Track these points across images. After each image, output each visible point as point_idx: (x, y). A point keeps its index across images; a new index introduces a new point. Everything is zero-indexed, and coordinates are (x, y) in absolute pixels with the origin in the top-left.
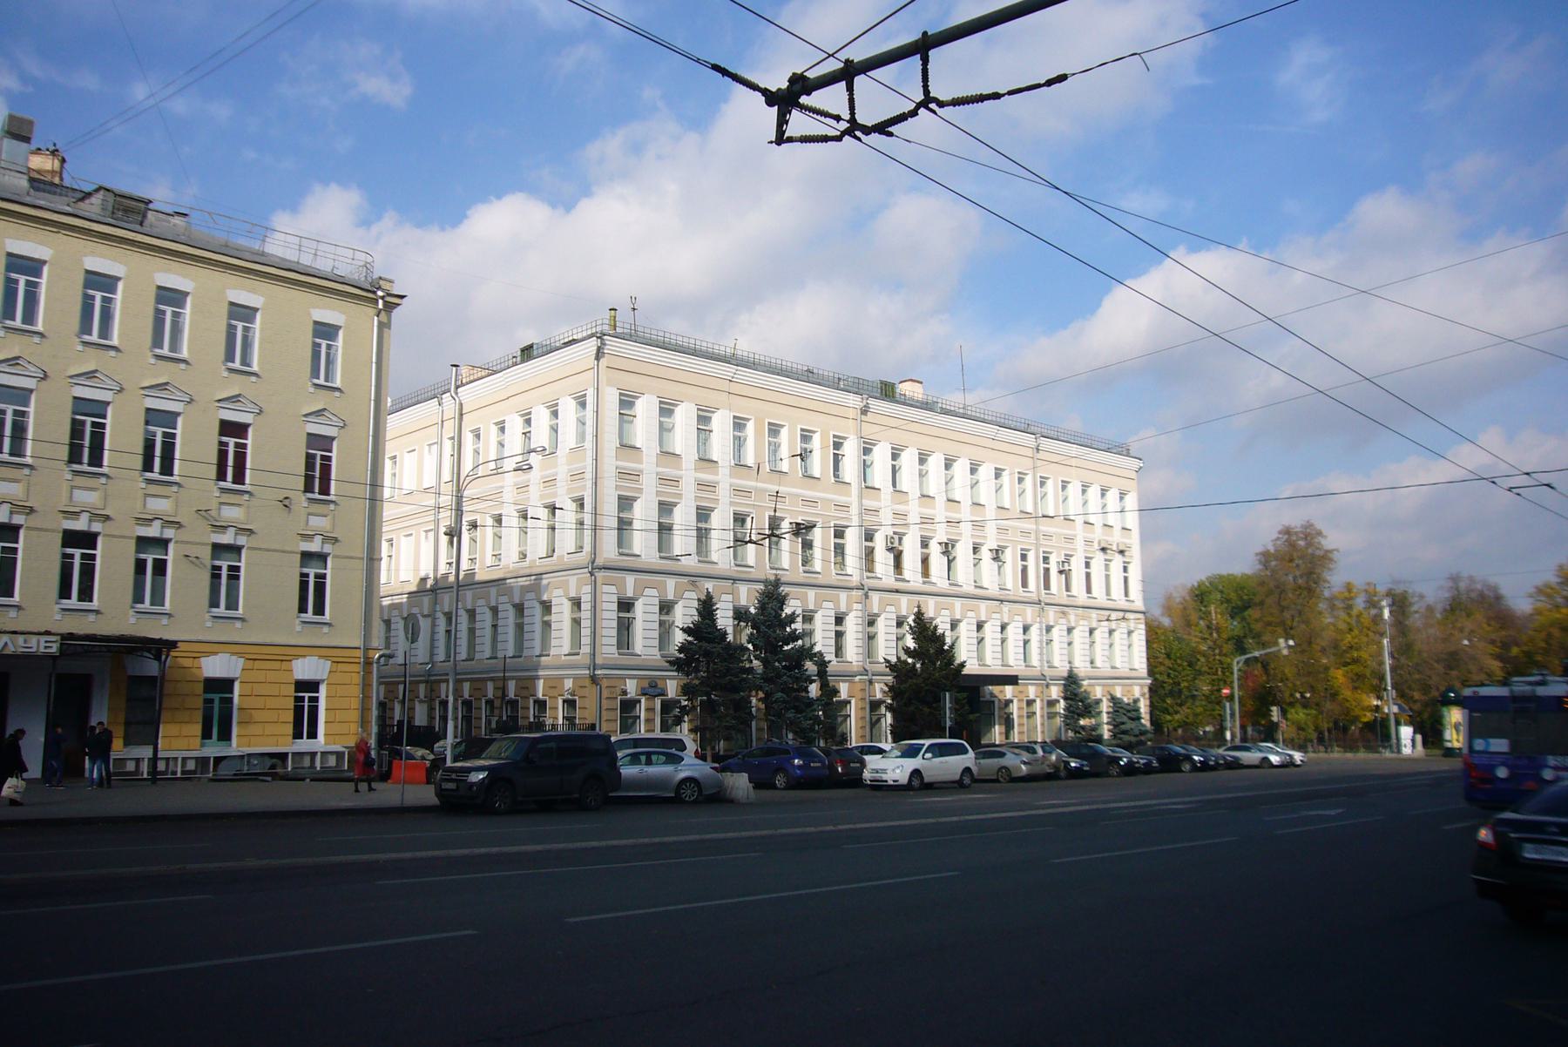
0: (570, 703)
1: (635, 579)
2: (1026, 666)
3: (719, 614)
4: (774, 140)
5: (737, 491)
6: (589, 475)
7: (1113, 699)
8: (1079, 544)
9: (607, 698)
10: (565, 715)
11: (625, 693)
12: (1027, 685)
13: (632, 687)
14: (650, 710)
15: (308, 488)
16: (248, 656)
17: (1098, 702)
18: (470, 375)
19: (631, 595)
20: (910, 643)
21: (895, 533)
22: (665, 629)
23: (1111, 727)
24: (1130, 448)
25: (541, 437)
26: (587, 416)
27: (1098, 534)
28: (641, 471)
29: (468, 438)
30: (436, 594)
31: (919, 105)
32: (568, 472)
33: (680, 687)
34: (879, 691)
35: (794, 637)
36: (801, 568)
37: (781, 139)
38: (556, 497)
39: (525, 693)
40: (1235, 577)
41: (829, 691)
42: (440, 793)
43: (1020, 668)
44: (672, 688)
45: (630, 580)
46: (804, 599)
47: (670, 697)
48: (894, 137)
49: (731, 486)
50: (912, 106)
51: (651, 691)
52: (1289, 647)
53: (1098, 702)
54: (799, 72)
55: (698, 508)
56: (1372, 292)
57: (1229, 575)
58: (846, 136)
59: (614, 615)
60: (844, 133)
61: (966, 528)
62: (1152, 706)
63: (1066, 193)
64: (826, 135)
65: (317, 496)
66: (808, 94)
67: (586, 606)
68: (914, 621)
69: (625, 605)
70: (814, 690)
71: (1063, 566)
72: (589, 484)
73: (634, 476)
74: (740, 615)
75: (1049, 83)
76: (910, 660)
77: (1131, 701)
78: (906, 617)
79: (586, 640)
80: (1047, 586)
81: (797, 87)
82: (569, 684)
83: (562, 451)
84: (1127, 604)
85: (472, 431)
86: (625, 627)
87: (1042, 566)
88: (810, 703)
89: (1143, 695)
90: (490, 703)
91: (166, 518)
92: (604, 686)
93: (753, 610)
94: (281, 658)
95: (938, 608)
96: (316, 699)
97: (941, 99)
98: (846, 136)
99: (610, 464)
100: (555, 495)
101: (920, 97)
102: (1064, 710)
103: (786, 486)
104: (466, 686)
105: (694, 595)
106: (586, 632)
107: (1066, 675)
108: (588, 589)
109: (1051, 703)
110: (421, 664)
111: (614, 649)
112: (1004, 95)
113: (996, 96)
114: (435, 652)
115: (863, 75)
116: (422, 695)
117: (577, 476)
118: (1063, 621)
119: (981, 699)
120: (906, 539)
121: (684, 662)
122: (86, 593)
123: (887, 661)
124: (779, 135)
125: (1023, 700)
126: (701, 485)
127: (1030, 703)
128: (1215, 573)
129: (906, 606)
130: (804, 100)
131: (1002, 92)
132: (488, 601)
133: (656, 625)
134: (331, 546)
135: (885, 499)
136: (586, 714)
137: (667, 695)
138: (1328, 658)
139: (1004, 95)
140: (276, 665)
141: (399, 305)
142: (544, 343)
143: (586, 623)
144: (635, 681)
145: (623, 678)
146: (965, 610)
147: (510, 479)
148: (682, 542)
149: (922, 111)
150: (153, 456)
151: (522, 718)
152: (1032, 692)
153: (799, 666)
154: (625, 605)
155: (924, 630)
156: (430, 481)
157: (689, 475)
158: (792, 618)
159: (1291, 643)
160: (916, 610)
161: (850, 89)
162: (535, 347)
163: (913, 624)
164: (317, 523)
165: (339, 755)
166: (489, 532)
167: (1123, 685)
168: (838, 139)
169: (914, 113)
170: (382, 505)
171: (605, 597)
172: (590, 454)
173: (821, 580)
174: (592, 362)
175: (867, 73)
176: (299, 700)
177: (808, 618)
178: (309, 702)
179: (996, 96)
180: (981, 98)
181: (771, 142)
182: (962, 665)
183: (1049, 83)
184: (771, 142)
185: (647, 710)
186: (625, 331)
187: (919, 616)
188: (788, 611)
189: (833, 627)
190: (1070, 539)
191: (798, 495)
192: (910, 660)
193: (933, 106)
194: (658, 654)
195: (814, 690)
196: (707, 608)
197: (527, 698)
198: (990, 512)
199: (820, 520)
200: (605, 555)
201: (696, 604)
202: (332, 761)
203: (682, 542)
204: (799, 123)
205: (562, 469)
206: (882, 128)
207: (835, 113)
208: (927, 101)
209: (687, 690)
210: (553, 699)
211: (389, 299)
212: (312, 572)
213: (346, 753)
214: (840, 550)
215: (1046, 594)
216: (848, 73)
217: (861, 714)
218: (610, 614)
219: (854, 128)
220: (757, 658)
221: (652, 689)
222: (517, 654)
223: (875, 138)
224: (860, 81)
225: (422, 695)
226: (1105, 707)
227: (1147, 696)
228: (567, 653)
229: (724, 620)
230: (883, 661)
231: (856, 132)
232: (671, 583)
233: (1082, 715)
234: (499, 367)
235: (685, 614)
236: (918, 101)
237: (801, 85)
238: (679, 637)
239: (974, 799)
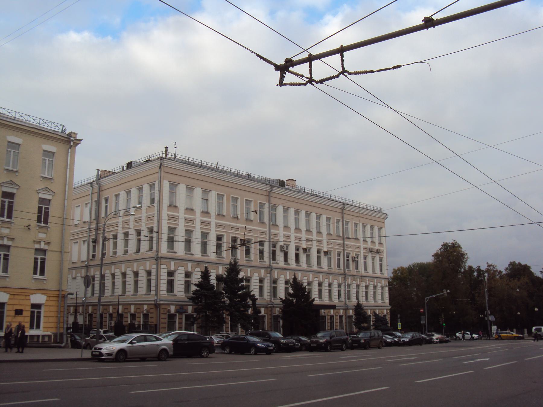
0: (146, 316)
1: (175, 263)
2: (339, 301)
3: (211, 278)
4: (279, 84)
5: (218, 225)
6: (156, 218)
7: (375, 315)
8: (362, 250)
10: (89, 320)
11: (169, 311)
12: (339, 309)
13: (173, 309)
14: (180, 319)
15: (39, 221)
16: (11, 293)
17: (370, 316)
18: (104, 174)
19: (190, 271)
20: (291, 291)
21: (284, 244)
22: (188, 284)
23: (374, 327)
24: (382, 209)
25: (134, 202)
26: (156, 193)
27: (369, 245)
28: (178, 217)
29: (103, 202)
30: (88, 268)
31: (340, 73)
32: (146, 217)
33: (193, 309)
34: (277, 311)
35: (243, 288)
36: (259, 260)
37: (281, 84)
38: (141, 227)
39: (126, 311)
40: (423, 264)
41: (257, 311)
42: (92, 355)
43: (337, 302)
44: (190, 309)
45: (173, 263)
46: (246, 272)
48: (323, 84)
49: (168, 215)
50: (337, 73)
52: (447, 293)
53: (370, 316)
54: (289, 58)
55: (202, 232)
56: (488, 146)
57: (421, 263)
58: (308, 83)
59: (166, 278)
60: (307, 82)
61: (315, 243)
62: (391, 318)
63: (392, 109)
64: (300, 86)
65: (42, 224)
66: (293, 67)
67: (153, 274)
68: (293, 281)
69: (171, 274)
70: (250, 311)
71: (355, 259)
72: (156, 222)
73: (193, 221)
74: (219, 278)
75: (394, 68)
76: (291, 299)
77: (382, 316)
78: (289, 280)
79: (153, 288)
80: (348, 267)
81: (288, 64)
82: (145, 307)
83: (144, 208)
84: (381, 275)
85: (105, 198)
86: (171, 284)
87: (346, 259)
88: (249, 317)
89: (387, 313)
90: (111, 315)
91: (9, 237)
93: (225, 276)
94: (25, 294)
95: (302, 276)
96: (39, 312)
97: (350, 72)
98: (308, 83)
99: (165, 212)
100: (141, 226)
101: (340, 70)
102: (355, 319)
103: (239, 224)
105: (199, 270)
106: (153, 285)
107: (356, 305)
108: (154, 266)
109: (350, 317)
110: (80, 298)
111: (165, 293)
112: (375, 72)
113: (372, 72)
114: (87, 293)
115: (319, 60)
116: (81, 311)
117: (150, 218)
118: (354, 282)
119: (320, 315)
120: (290, 248)
121: (196, 298)
122: (42, 273)
123: (281, 299)
124: (281, 82)
125: (337, 316)
126: (203, 223)
127: (341, 317)
128: (416, 262)
129: (289, 276)
130: (291, 69)
131: (374, 70)
132: (111, 271)
134: (48, 246)
135: (281, 232)
136: (153, 320)
139: (375, 72)
140: (23, 297)
141: (79, 144)
142: (137, 161)
143: (153, 281)
145: (169, 305)
146: (127, 267)
147: (121, 220)
148: (196, 248)
149: (341, 76)
150: (4, 209)
151: (338, 322)
152: (341, 312)
153: (245, 300)
154: (171, 274)
155: (296, 285)
156: (87, 219)
157: (198, 218)
158: (242, 280)
159: (448, 291)
160: (293, 277)
161: (311, 66)
162: (133, 163)
163: (292, 283)
164: (42, 236)
165: (49, 336)
166: (111, 241)
167: (379, 309)
168: (305, 84)
169: (337, 76)
170: (157, 237)
172: (156, 209)
173: (253, 264)
174: (157, 169)
175: (321, 59)
176: (33, 312)
177: (248, 280)
178: (37, 313)
179: (372, 72)
180: (366, 72)
181: (277, 85)
182: (313, 300)
183: (394, 68)
184: (277, 85)
185: (179, 319)
186: (172, 157)
187: (295, 279)
188: (240, 276)
189: (258, 284)
190: (358, 247)
191: (230, 225)
192: (291, 299)
193: (346, 74)
195: (250, 311)
196: (205, 275)
197: (106, 313)
198: (325, 237)
199: (253, 238)
201: (200, 273)
202: (46, 339)
203: (196, 248)
204: (289, 78)
205: (144, 215)
206: (321, 82)
207: (301, 74)
208: (343, 72)
209: (195, 310)
210: (126, 314)
211: (75, 141)
212: (39, 257)
213: (53, 336)
214: (261, 252)
215: (338, 269)
216: (310, 59)
217: (270, 321)
218: (164, 278)
219: (311, 80)
220: (227, 297)
221: (181, 309)
222: (123, 294)
223: (319, 85)
224: (314, 62)
225: (81, 311)
226: (372, 319)
227: (389, 314)
228: (132, 294)
229: (213, 280)
230: (279, 299)
231: (312, 82)
232: (190, 265)
233: (363, 322)
234: (117, 171)
235: (196, 278)
236: (340, 72)
237: (290, 63)
238: (194, 288)
239: (350, 356)
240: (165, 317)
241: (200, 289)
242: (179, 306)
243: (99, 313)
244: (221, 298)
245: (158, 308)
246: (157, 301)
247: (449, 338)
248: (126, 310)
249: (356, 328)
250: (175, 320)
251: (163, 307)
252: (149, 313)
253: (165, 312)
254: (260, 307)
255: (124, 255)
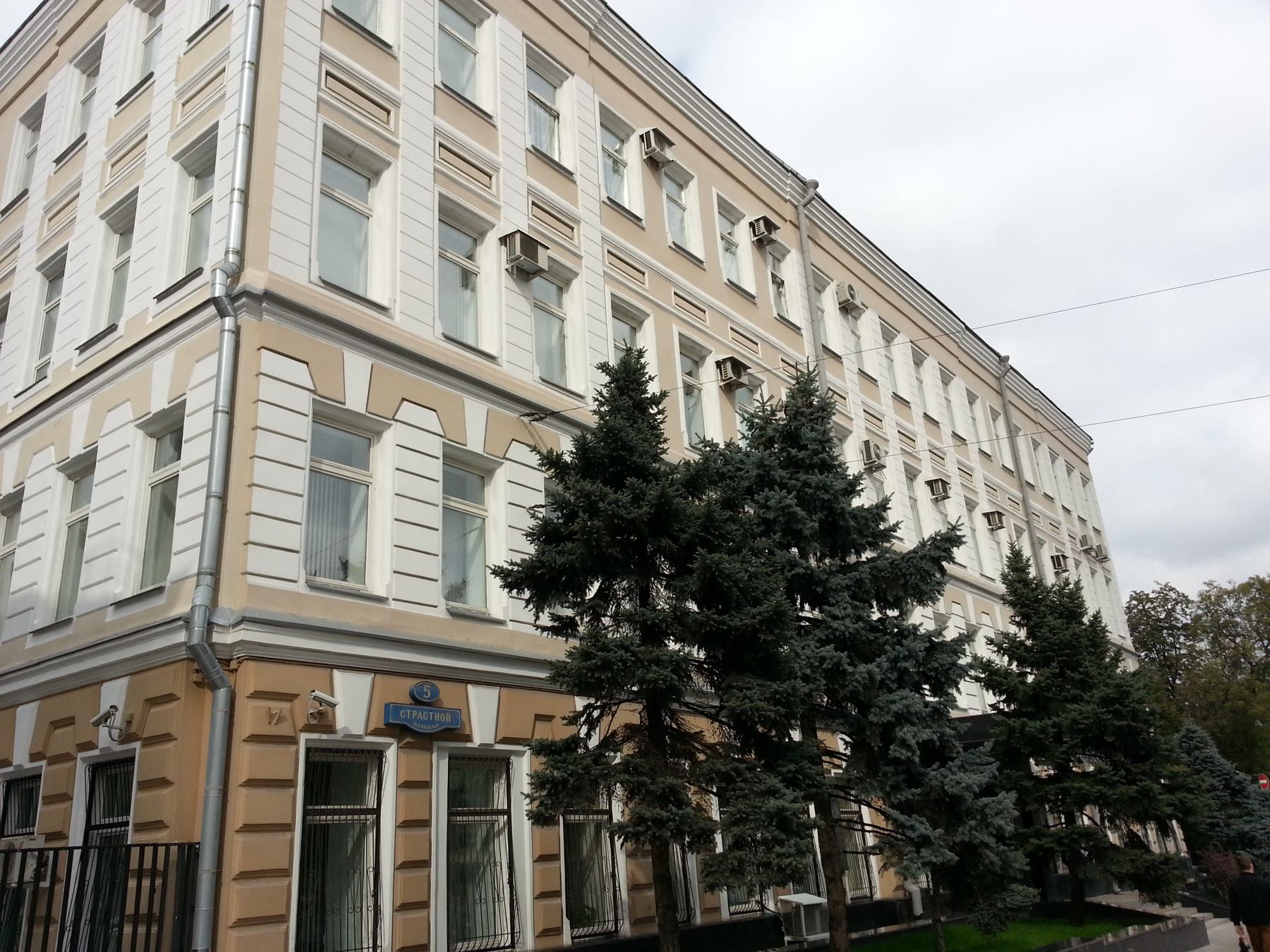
9: (254, 739)
11: (322, 720)
14: (414, 785)
47: (477, 740)
51: (420, 719)
61: (1089, 699)
92: (243, 692)
104: (592, 592)
111: (293, 566)
133: (434, 517)
137: (469, 738)
138: (1240, 685)
144: (366, 679)
171: (268, 389)
194: (442, 603)
200: (276, 266)
240: (286, 775)
241: (658, 575)
242: (411, 683)
243: (1059, 849)
244: (1015, 663)
245: (214, 687)
246: (210, 626)
247: (940, 831)
248: (540, 725)
249: (1114, 833)
250: (372, 804)
251: (250, 678)
252: (137, 745)
253: (285, 729)
254: (411, 704)
255: (229, 47)
